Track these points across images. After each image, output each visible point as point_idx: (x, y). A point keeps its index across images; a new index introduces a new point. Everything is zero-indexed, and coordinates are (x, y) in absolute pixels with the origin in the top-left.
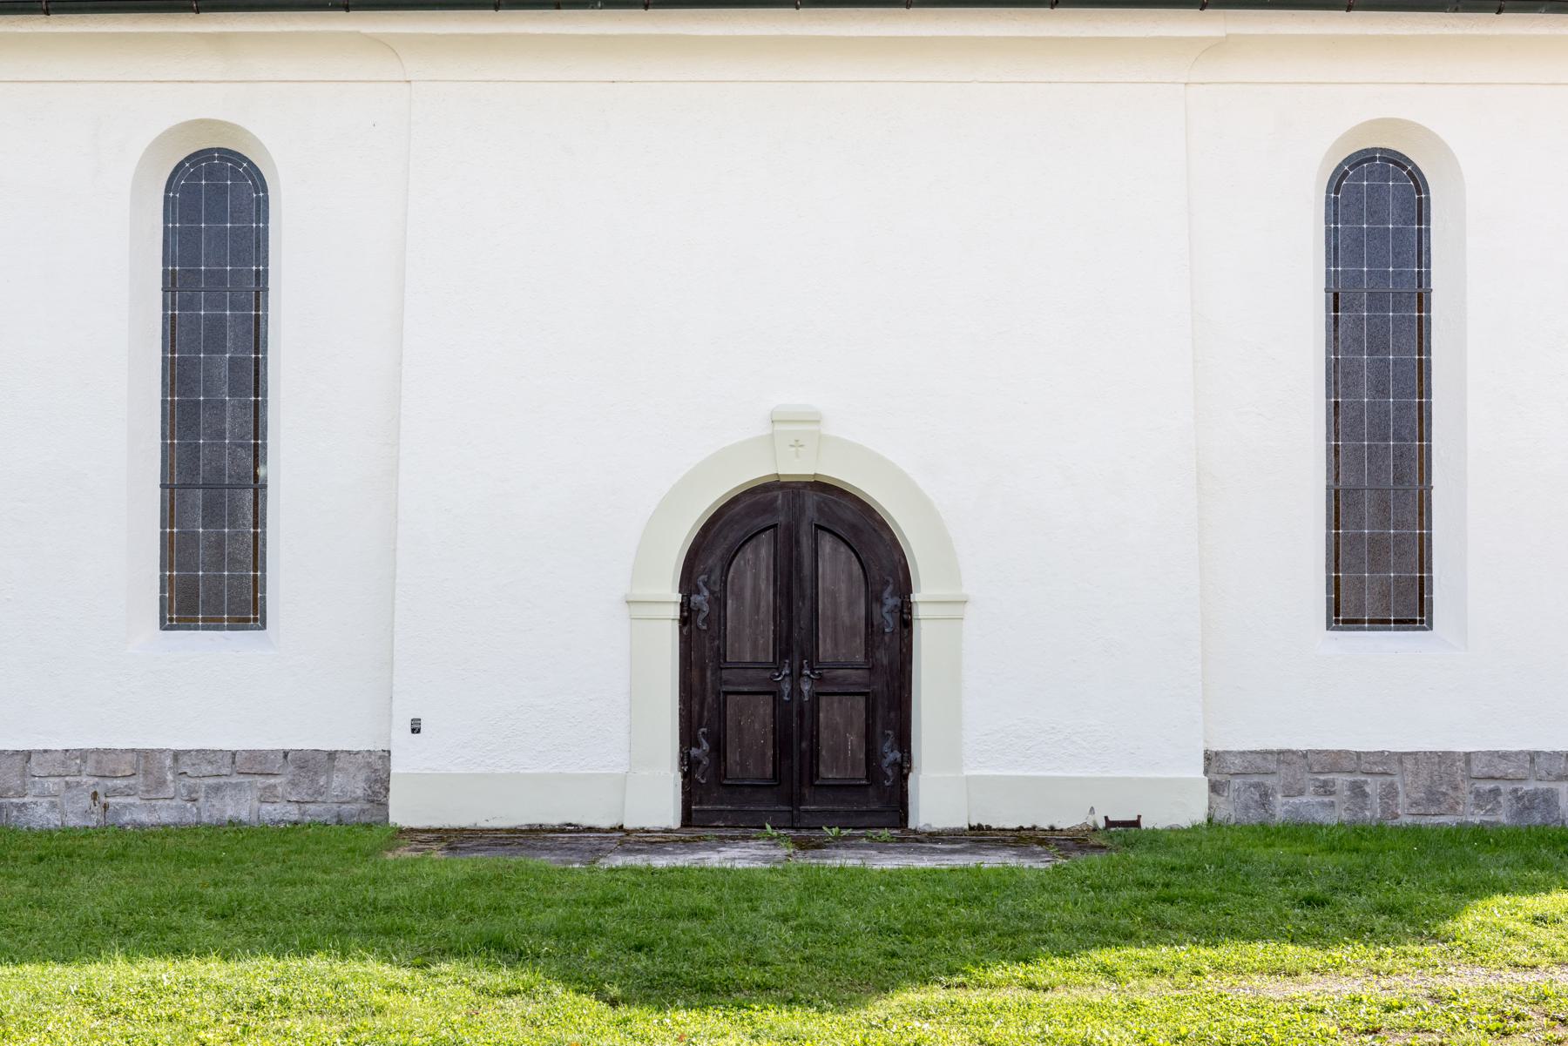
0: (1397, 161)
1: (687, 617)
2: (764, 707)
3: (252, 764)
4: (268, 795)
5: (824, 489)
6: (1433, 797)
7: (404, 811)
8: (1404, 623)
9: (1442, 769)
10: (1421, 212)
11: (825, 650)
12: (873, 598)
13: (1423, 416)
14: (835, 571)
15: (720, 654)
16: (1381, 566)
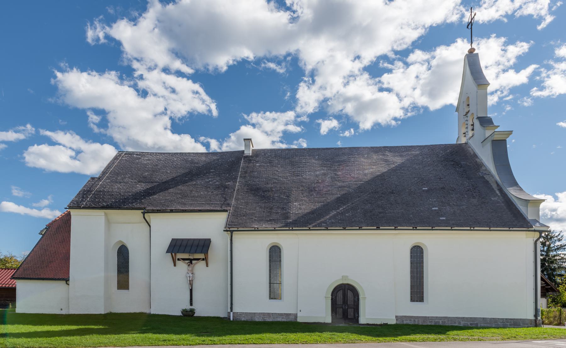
0: (419, 247)
1: (332, 299)
2: (341, 309)
3: (281, 315)
4: (283, 318)
5: (348, 285)
6: (424, 322)
7: (299, 320)
8: (420, 301)
9: (425, 318)
10: (422, 253)
11: (349, 303)
12: (354, 297)
13: (423, 277)
14: (350, 294)
15: (336, 304)
16: (417, 293)
